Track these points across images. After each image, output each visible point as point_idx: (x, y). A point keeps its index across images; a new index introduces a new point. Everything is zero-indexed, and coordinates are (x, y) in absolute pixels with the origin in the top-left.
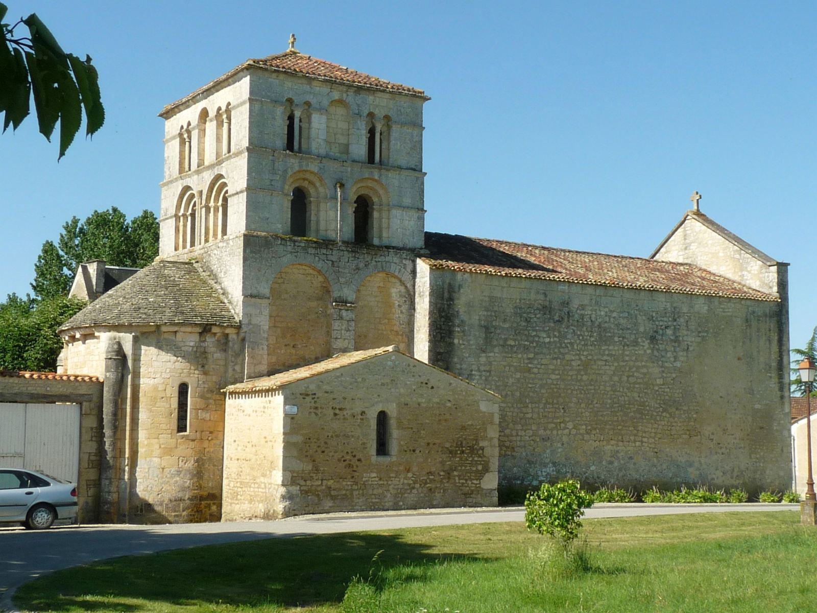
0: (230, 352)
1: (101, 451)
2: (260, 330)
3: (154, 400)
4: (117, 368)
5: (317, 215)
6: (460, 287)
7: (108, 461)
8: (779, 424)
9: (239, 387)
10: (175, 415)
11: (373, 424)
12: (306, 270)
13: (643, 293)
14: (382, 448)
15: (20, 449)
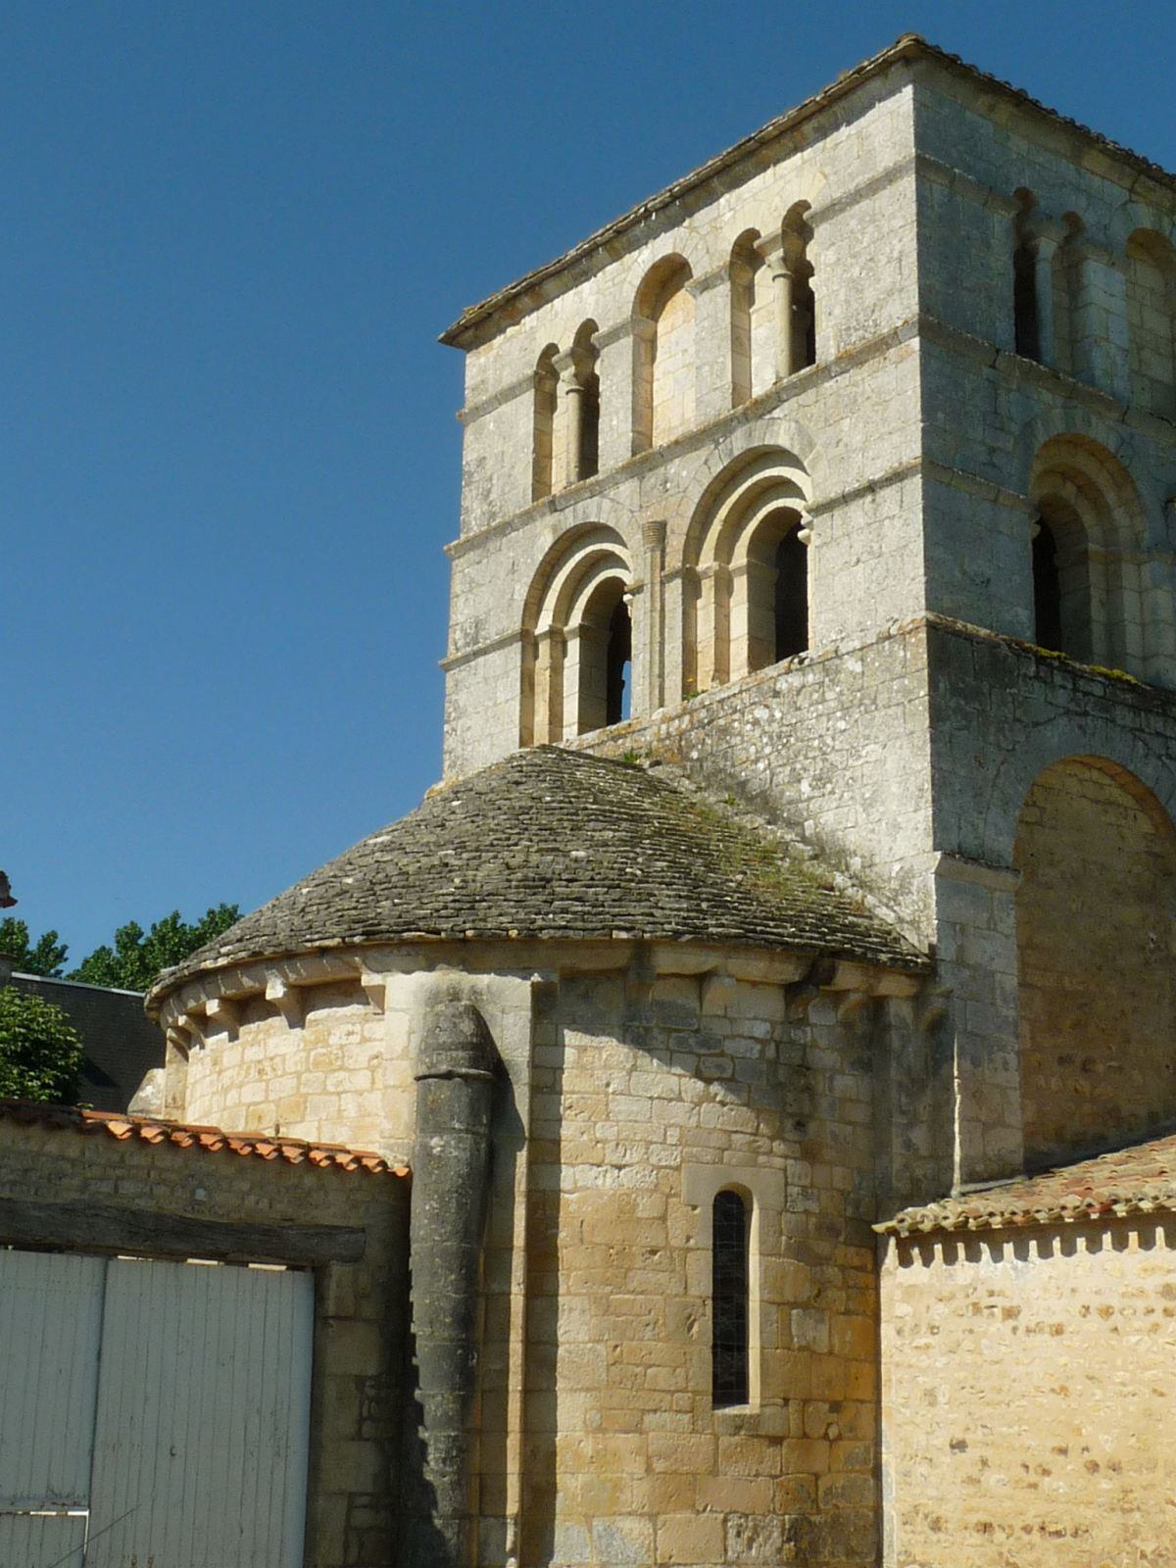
0: (894, 1073)
1: (400, 1484)
2: (993, 989)
3: (618, 1262)
4: (474, 1114)
5: (1112, 603)
7: (439, 1533)
9: (928, 1215)
10: (703, 1327)
12: (1102, 786)
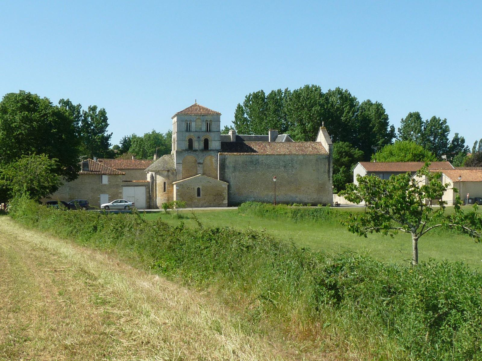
3: (159, 185)
6: (227, 158)
8: (328, 186)
10: (163, 188)
11: (196, 190)
13: (281, 156)
14: (199, 195)
15: (133, 196)
